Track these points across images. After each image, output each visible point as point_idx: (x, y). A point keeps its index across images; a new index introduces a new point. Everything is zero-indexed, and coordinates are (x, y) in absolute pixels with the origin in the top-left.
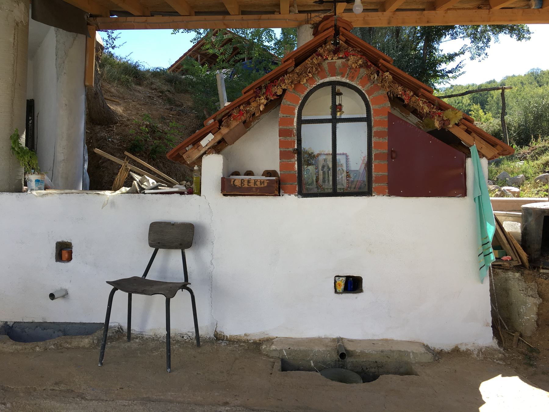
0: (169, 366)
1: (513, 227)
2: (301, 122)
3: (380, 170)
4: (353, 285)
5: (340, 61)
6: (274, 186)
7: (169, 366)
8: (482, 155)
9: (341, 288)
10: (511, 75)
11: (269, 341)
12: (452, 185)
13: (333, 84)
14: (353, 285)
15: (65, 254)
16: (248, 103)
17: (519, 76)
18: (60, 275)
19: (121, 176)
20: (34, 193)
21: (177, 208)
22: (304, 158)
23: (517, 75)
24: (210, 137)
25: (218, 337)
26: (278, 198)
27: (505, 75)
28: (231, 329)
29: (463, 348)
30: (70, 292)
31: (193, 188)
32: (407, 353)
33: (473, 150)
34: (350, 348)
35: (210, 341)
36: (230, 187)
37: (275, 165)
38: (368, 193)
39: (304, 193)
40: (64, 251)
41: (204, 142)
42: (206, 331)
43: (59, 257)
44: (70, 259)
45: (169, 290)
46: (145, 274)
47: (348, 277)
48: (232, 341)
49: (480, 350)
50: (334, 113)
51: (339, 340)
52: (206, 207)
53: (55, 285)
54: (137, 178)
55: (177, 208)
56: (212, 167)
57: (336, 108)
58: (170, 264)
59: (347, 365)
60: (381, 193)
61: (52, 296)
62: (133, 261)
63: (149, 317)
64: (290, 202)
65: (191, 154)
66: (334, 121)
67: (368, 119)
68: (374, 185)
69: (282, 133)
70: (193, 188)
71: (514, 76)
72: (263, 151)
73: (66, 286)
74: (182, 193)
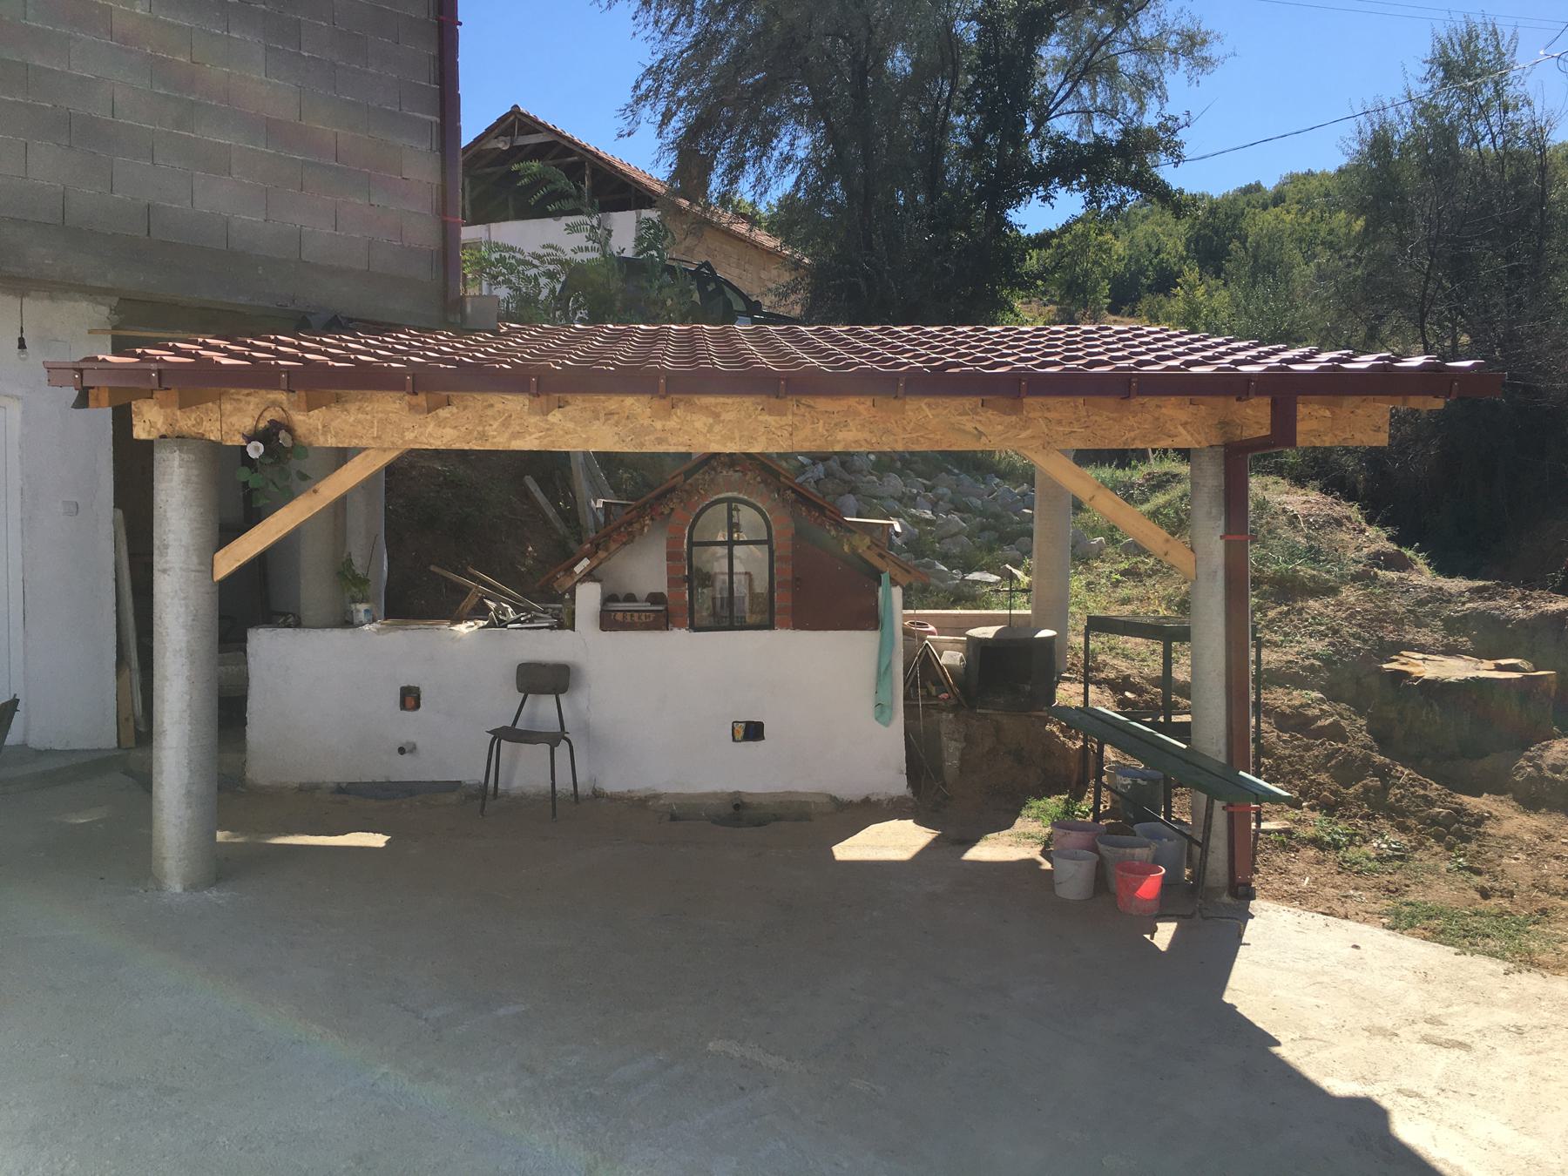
0: (554, 815)
1: (951, 658)
2: (691, 544)
3: (782, 600)
4: (753, 731)
5: (737, 475)
6: (660, 615)
7: (554, 815)
8: (894, 583)
9: (739, 735)
10: (1302, 170)
11: (657, 797)
12: (868, 618)
13: (729, 500)
14: (753, 731)
15: (410, 701)
16: (630, 524)
17: (1324, 174)
18: (409, 726)
19: (470, 602)
20: (366, 627)
21: (546, 646)
22: (698, 578)
23: (1317, 170)
24: (585, 562)
25: (597, 795)
26: (666, 633)
27: (1286, 172)
28: (613, 784)
29: (874, 798)
30: (419, 745)
31: (565, 622)
32: (807, 803)
33: (885, 578)
34: (746, 800)
35: (588, 798)
36: (608, 621)
37: (662, 587)
38: (770, 626)
39: (695, 628)
40: (410, 698)
41: (578, 569)
42: (584, 787)
43: (403, 706)
44: (417, 706)
45: (554, 739)
46: (515, 723)
47: (748, 724)
48: (615, 798)
49: (891, 800)
50: (730, 535)
51: (738, 793)
52: (584, 644)
53: (405, 737)
54: (492, 605)
55: (546, 646)
56: (588, 597)
57: (733, 526)
58: (544, 709)
59: (739, 813)
60: (784, 626)
61: (402, 751)
62: (502, 705)
63: (527, 770)
64: (679, 638)
65: (564, 582)
66: (730, 543)
67: (768, 541)
68: (777, 617)
69: (670, 557)
70: (565, 622)
71: (1310, 174)
72: (646, 569)
73: (413, 739)
74: (551, 628)
